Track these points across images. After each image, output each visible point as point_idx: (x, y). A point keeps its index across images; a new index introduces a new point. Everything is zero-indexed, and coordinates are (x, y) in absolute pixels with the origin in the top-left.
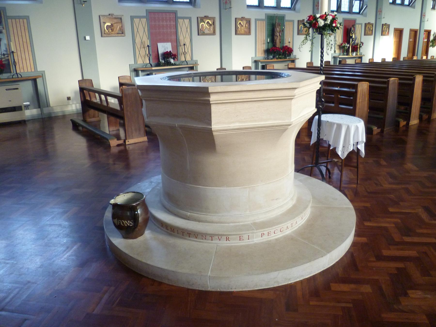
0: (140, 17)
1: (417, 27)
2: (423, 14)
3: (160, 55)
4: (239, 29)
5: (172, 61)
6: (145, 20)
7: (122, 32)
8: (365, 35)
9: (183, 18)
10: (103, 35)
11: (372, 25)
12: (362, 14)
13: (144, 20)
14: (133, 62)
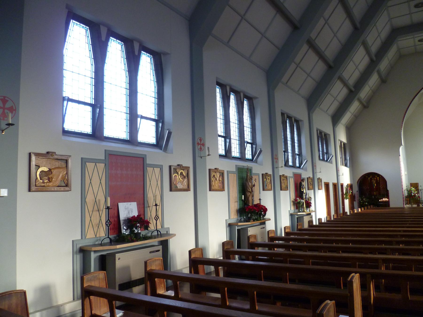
0: (96, 161)
1: (336, 182)
2: (275, 156)
3: (122, 222)
4: (213, 183)
5: (143, 233)
6: (103, 165)
7: (66, 185)
8: (308, 189)
9: (154, 166)
10: (33, 188)
12: (302, 169)
13: (101, 166)
14: (78, 237)
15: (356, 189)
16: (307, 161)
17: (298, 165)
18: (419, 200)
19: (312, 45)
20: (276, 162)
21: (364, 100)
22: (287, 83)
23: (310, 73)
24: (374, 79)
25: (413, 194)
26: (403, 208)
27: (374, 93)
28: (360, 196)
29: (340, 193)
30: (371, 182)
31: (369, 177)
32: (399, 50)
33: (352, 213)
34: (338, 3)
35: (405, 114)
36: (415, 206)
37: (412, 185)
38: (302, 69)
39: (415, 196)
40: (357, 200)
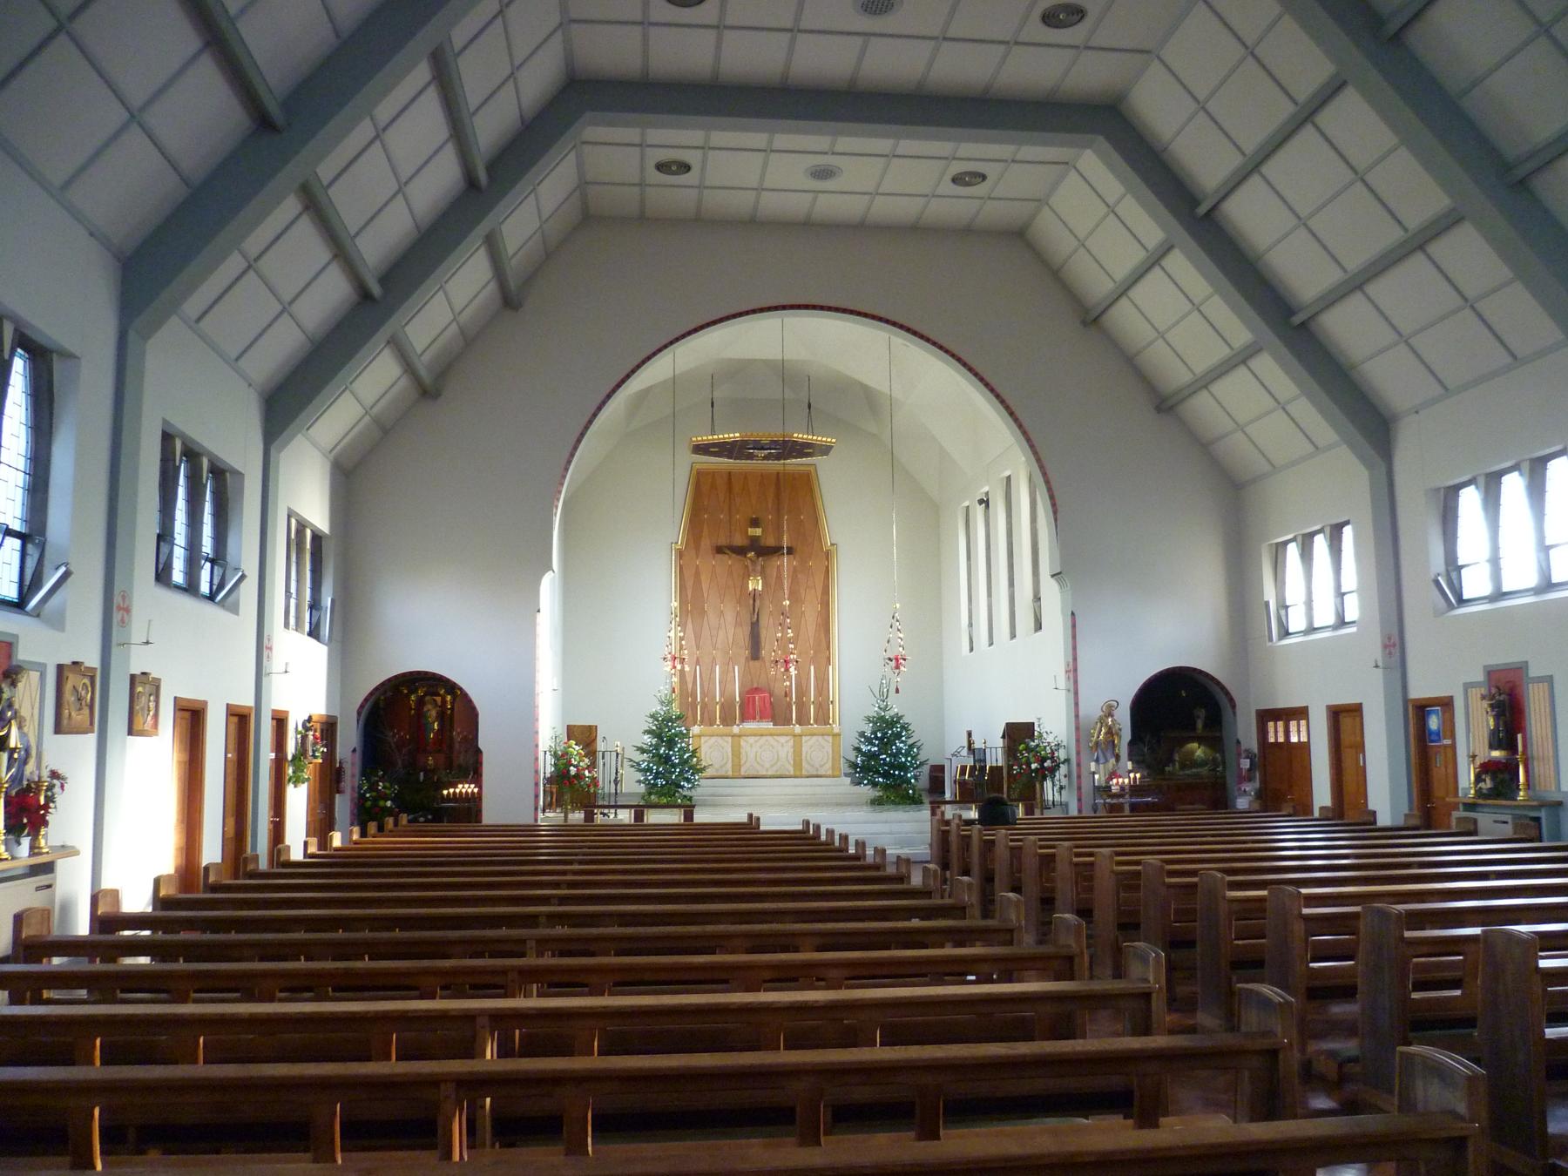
1: (247, 700)
2: (117, 600)
8: (58, 730)
11: (90, 674)
12: (37, 613)
15: (349, 739)
16: (66, 575)
17: (205, 588)
18: (595, 794)
19: (315, 205)
20: (123, 621)
21: (426, 358)
22: (199, 319)
23: (143, 108)
24: (466, 283)
25: (573, 770)
26: (531, 830)
27: (469, 343)
28: (364, 773)
29: (267, 755)
30: (420, 714)
31: (411, 692)
32: (583, 184)
33: (313, 849)
34: (429, 84)
35: (575, 448)
36: (577, 817)
37: (572, 732)
38: (261, 277)
39: (579, 776)
40: (348, 790)
